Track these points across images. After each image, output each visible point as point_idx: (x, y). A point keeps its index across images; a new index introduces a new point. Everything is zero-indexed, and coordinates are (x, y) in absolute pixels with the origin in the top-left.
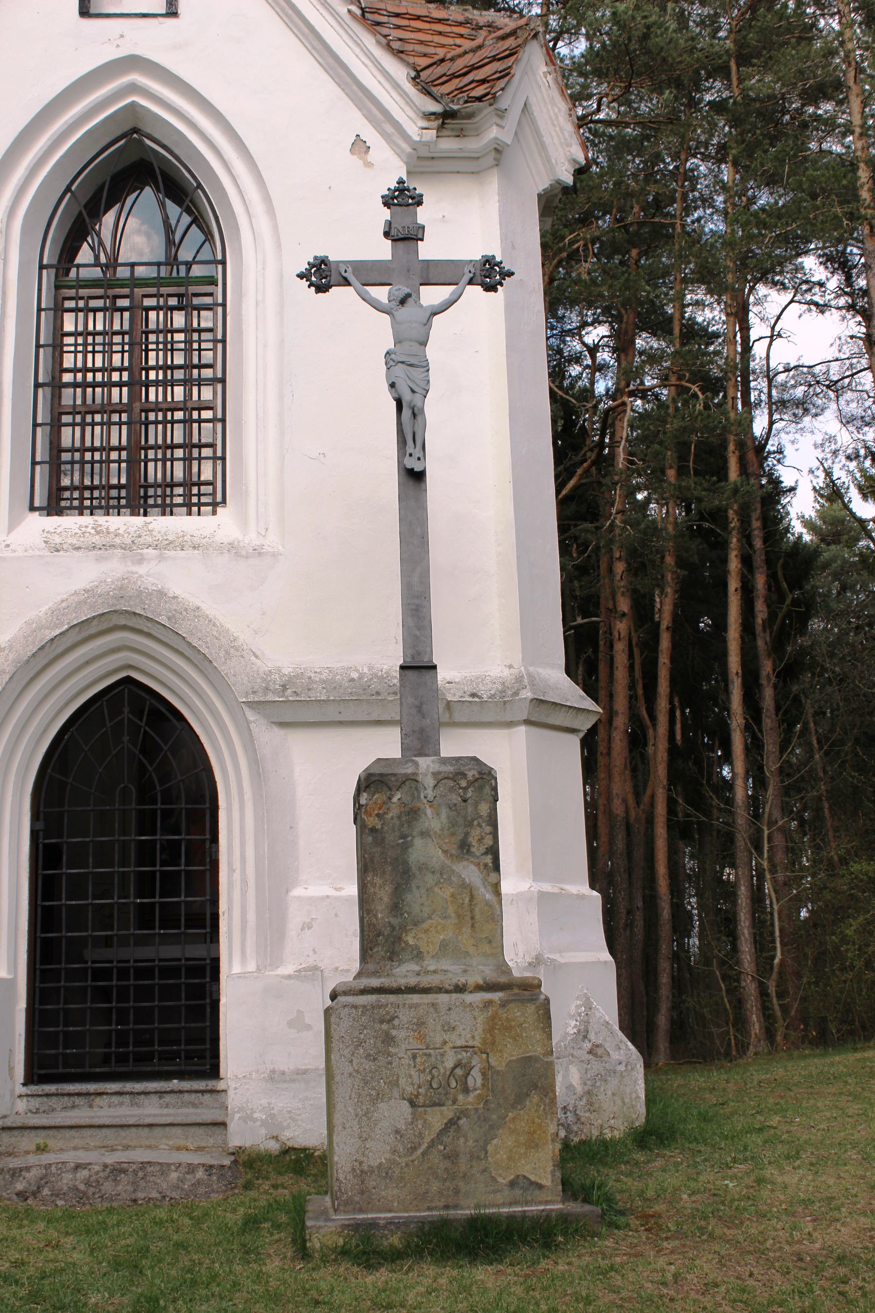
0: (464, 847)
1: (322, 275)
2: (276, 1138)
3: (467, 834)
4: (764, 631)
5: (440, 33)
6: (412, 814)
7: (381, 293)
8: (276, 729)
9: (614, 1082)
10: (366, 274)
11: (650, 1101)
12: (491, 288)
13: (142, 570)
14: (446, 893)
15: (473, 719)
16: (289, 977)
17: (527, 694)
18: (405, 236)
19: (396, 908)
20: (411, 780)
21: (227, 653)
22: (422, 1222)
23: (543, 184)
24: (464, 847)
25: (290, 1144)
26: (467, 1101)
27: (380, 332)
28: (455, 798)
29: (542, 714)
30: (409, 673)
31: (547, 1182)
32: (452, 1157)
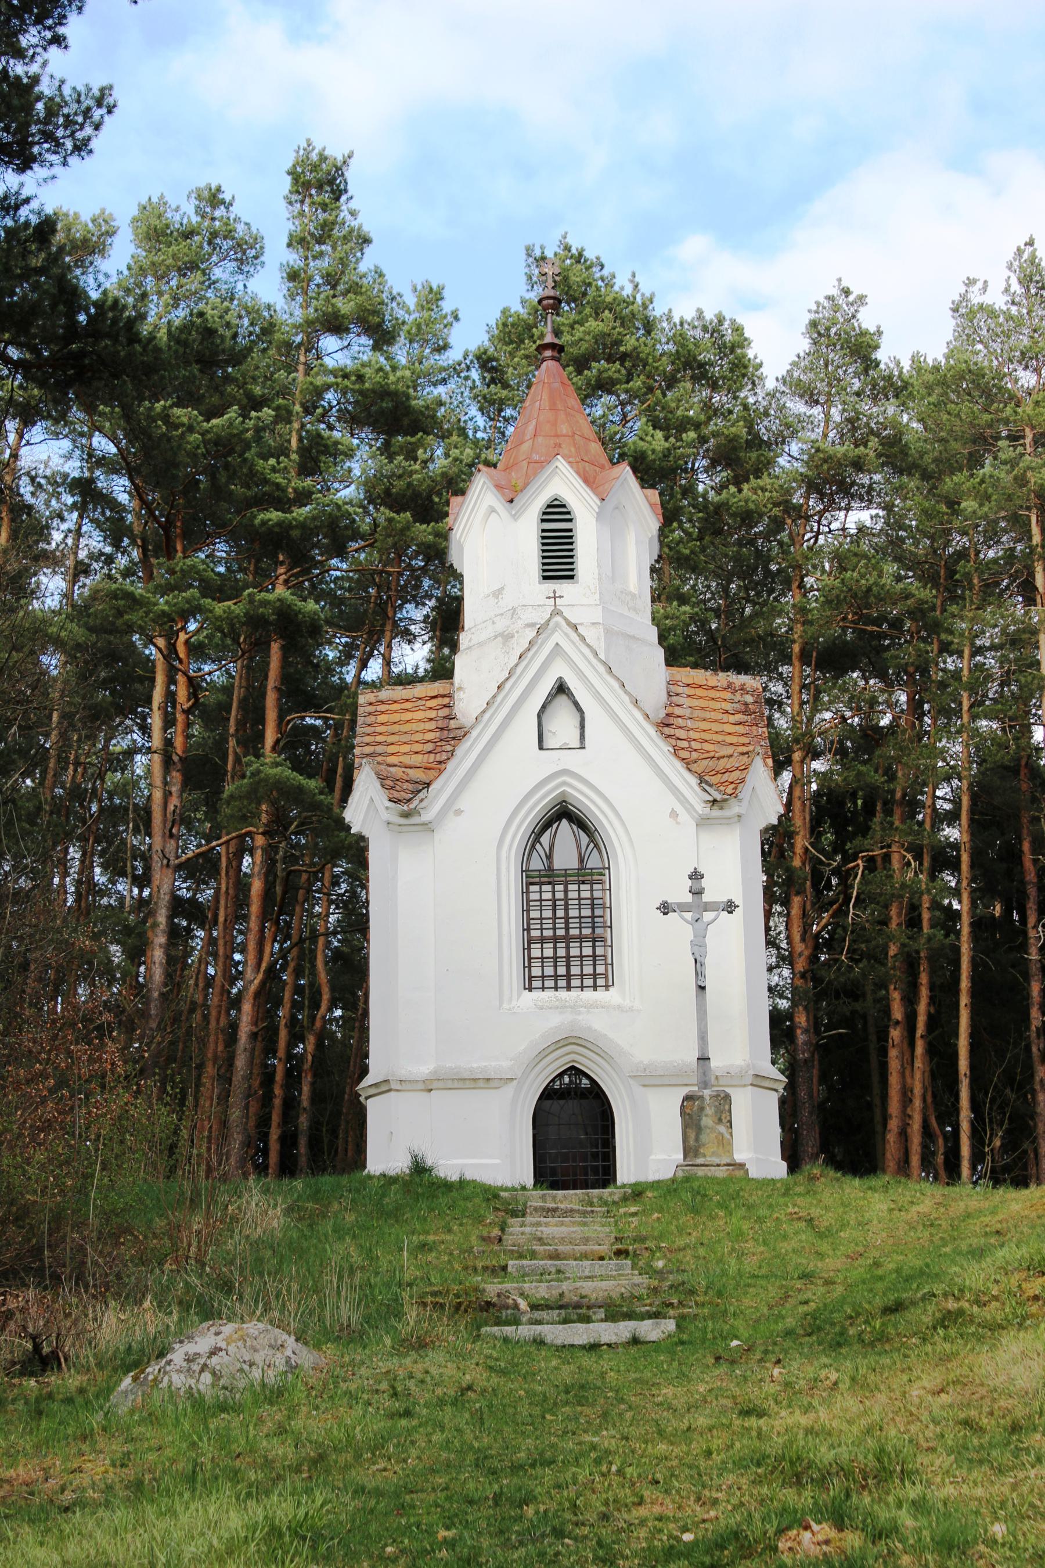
0: (720, 1120)
1: (665, 908)
4: (1038, 1037)
6: (702, 1109)
7: (688, 916)
10: (683, 908)
12: (730, 912)
13: (580, 1018)
14: (713, 1136)
17: (751, 1072)
18: (697, 892)
19: (697, 1139)
20: (701, 1098)
23: (763, 825)
24: (720, 1120)
27: (688, 932)
29: (759, 1081)
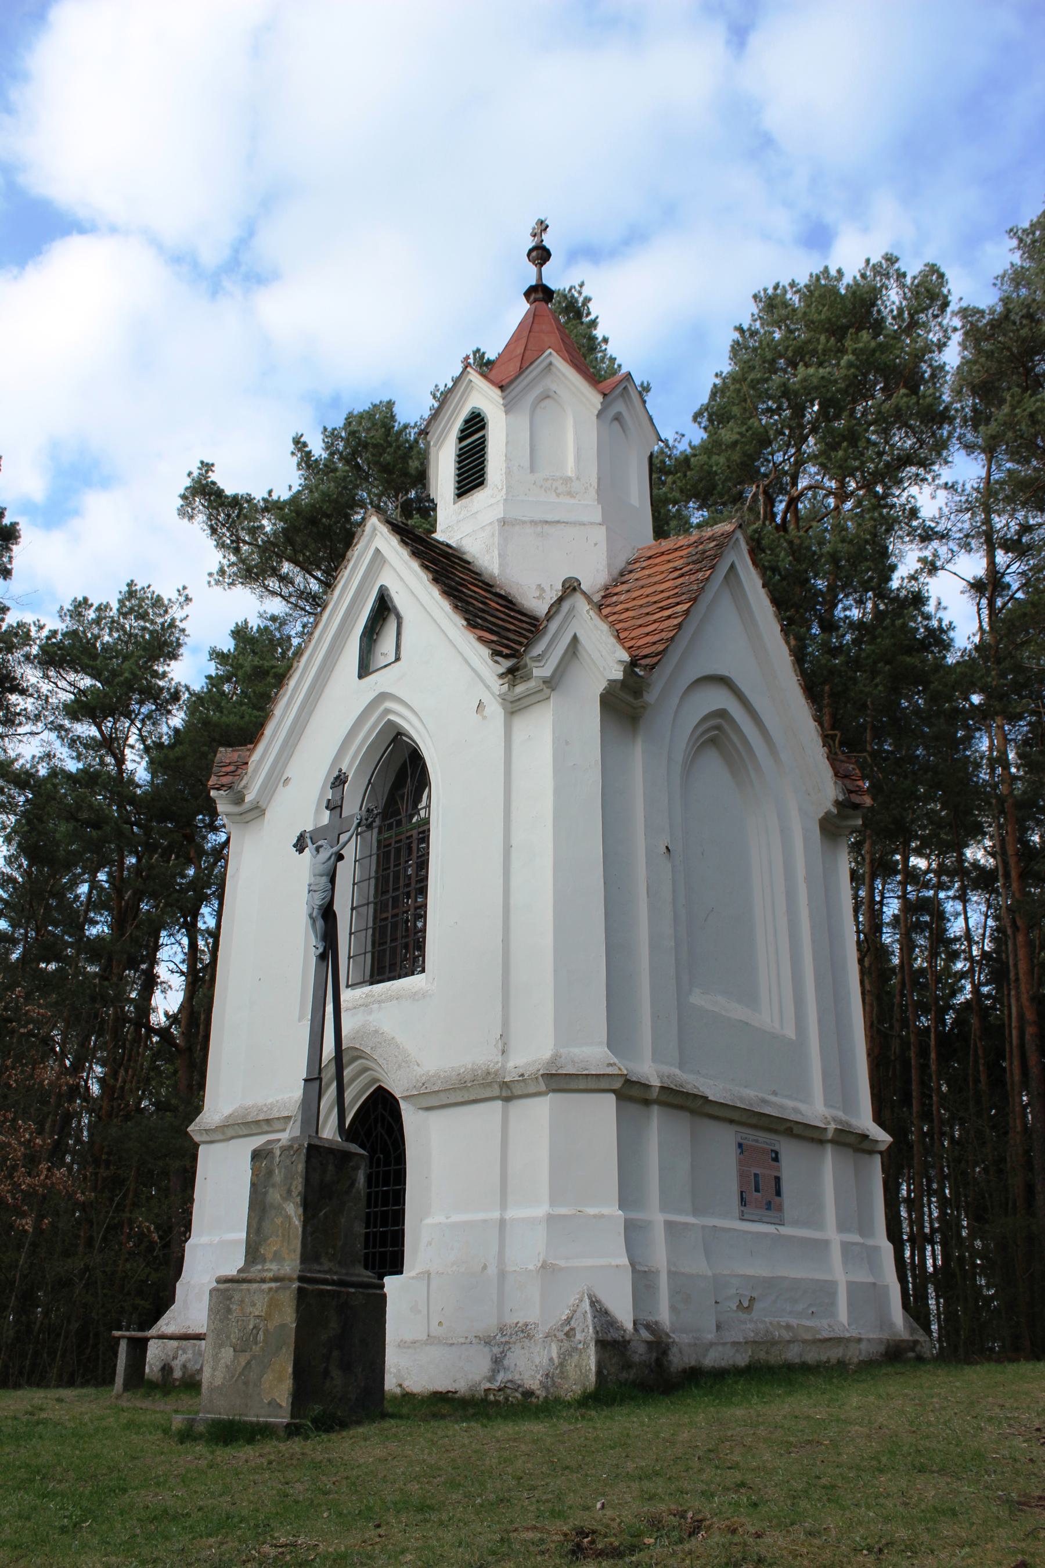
2: (400, 1385)
3: (291, 1184)
5: (669, 561)
8: (420, 1111)
9: (576, 1357)
11: (599, 1373)
15: (526, 1092)
16: (413, 1278)
21: (400, 1066)
22: (213, 1420)
23: (601, 686)
25: (408, 1390)
26: (256, 1349)
28: (288, 1162)
30: (308, 1083)
31: (284, 1404)
32: (246, 1383)
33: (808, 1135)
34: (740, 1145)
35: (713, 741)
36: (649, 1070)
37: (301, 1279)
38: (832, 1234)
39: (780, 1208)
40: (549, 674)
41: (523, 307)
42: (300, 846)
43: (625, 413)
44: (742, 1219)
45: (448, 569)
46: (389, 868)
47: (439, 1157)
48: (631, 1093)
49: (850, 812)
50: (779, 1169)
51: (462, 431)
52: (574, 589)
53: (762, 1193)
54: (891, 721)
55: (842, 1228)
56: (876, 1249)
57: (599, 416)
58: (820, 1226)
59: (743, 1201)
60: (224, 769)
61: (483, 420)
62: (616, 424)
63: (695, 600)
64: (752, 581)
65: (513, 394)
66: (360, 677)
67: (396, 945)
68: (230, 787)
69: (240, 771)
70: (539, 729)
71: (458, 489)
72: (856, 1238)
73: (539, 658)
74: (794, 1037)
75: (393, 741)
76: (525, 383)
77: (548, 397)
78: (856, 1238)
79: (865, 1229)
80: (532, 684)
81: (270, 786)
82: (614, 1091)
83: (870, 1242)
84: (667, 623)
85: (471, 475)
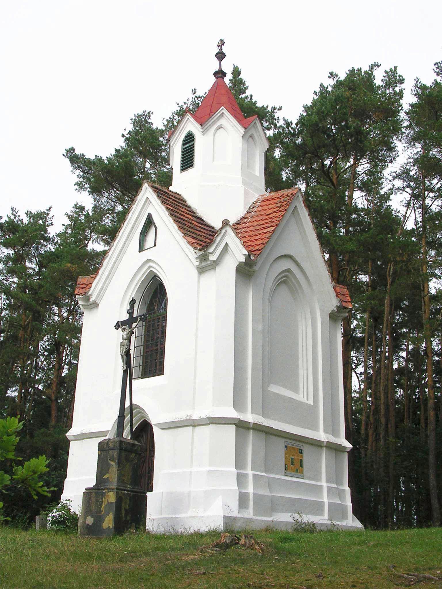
33: (317, 444)
34: (286, 447)
35: (284, 282)
36: (250, 418)
37: (117, 489)
38: (324, 483)
39: (302, 472)
40: (215, 259)
41: (213, 79)
42: (117, 326)
43: (255, 135)
44: (286, 475)
45: (177, 207)
46: (150, 331)
47: (166, 448)
48: (241, 426)
49: (342, 310)
50: (302, 457)
51: (184, 141)
52: (227, 224)
53: (295, 464)
54: (372, 263)
55: (328, 481)
56: (344, 490)
57: (243, 137)
58: (319, 480)
59: (286, 469)
60: (81, 286)
61: (193, 137)
62: (251, 139)
63: (277, 225)
64: (304, 213)
65: (206, 127)
66: (139, 252)
67: (151, 361)
68: (84, 294)
69: (88, 287)
70: (210, 279)
71: (182, 167)
72: (335, 486)
73: (212, 253)
74: (312, 404)
75: (153, 278)
76: (213, 121)
77: (222, 127)
78: (335, 486)
79: (339, 482)
80: (209, 262)
81: (101, 294)
82: (235, 424)
83: (341, 488)
84: (264, 236)
85: (188, 162)
